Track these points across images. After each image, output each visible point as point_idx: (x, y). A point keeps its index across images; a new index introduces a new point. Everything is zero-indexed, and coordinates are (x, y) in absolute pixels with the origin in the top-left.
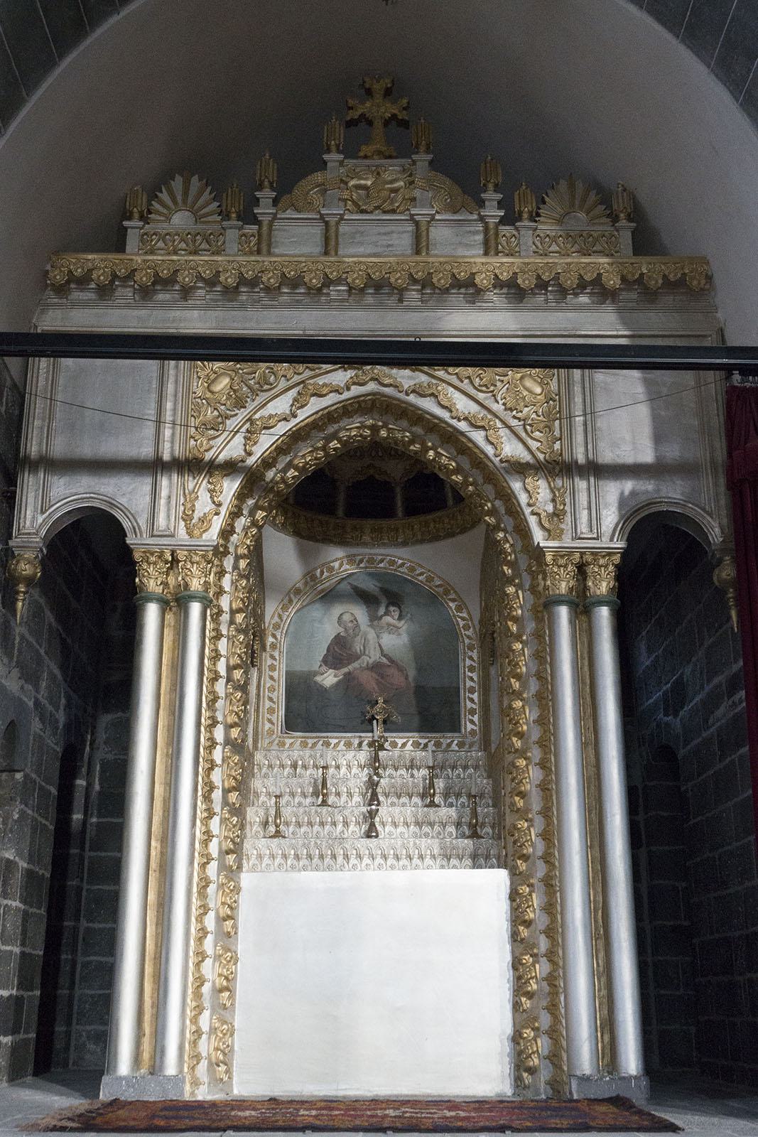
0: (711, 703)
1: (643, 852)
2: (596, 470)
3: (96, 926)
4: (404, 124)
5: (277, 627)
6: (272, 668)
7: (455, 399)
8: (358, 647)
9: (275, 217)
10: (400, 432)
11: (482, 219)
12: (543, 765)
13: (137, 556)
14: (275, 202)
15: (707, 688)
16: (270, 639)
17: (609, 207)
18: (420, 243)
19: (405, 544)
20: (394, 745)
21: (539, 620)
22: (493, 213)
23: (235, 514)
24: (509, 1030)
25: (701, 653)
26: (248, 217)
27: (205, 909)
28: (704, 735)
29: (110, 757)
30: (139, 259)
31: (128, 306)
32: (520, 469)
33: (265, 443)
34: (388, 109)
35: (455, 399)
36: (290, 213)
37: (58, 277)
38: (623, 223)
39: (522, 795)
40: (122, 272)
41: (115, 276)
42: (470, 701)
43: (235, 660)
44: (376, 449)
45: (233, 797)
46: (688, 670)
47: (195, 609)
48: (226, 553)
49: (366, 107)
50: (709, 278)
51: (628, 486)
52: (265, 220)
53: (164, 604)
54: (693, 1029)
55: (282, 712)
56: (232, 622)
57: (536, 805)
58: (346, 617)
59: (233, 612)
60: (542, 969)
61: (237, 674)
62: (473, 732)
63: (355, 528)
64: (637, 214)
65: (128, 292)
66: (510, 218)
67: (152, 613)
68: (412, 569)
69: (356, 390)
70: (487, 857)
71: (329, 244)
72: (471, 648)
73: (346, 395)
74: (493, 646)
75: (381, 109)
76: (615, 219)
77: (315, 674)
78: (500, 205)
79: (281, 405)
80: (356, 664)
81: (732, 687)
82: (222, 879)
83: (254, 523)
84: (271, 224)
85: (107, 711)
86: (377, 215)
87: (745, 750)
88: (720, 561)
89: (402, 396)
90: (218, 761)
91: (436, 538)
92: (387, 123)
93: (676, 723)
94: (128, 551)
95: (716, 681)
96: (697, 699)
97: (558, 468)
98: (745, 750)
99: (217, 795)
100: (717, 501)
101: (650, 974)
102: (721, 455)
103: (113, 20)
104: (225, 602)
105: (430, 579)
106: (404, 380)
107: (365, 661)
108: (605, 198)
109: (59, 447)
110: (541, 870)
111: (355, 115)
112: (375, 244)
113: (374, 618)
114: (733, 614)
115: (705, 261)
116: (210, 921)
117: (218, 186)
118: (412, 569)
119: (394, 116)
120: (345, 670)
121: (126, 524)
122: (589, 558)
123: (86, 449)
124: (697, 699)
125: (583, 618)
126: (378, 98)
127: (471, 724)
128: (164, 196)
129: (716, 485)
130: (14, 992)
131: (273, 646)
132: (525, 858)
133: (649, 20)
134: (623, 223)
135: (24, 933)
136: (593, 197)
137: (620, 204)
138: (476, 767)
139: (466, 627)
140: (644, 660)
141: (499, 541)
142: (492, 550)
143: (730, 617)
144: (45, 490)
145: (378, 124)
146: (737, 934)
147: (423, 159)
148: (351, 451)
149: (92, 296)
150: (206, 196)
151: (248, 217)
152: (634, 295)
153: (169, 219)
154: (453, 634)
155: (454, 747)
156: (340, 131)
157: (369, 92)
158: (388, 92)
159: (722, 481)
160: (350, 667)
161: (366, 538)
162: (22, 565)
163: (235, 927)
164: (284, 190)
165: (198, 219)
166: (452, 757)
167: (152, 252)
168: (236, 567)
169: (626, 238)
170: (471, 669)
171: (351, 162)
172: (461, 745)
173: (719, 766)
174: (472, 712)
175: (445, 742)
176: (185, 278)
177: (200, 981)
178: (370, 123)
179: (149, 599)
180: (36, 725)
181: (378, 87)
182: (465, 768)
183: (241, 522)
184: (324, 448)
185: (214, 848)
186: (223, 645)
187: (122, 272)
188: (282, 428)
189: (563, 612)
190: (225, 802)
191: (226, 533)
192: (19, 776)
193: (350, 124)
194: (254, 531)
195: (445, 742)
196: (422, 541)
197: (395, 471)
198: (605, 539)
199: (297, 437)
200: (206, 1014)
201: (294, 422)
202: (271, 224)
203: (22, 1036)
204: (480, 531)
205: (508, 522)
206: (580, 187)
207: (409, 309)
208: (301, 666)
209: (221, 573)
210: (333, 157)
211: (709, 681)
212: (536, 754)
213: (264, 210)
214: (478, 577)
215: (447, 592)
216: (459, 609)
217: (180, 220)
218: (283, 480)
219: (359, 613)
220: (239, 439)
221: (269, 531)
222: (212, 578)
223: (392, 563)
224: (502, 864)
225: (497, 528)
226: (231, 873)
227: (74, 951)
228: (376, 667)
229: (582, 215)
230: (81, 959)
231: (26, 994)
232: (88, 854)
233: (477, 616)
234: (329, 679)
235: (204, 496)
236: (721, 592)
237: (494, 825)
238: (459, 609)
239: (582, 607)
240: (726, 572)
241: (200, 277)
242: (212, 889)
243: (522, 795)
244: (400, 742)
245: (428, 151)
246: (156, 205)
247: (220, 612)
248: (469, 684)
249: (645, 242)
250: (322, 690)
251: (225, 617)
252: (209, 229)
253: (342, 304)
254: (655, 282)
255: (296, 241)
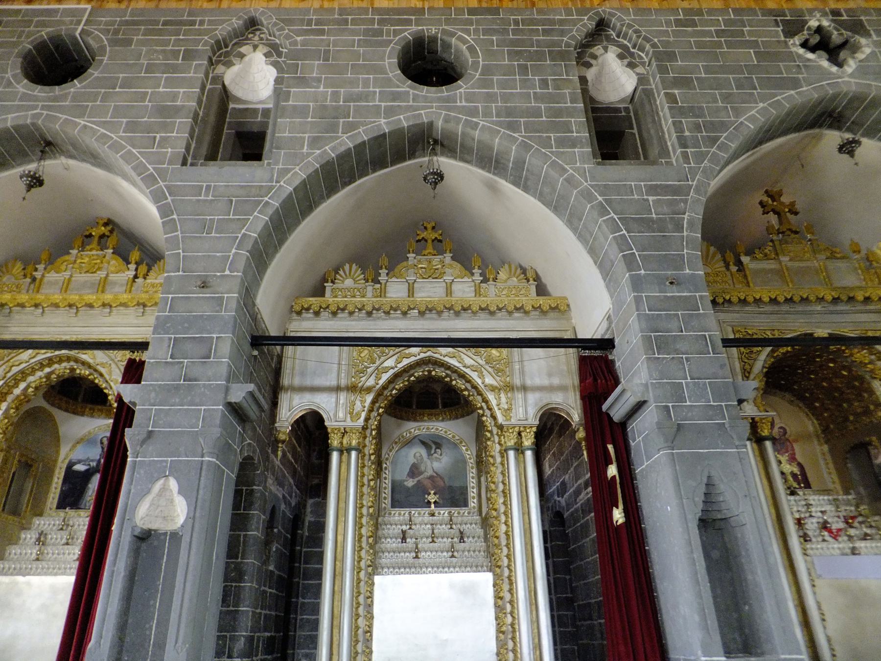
0: (577, 493)
1: (550, 561)
2: (524, 388)
3: (306, 601)
4: (440, 241)
5: (387, 459)
6: (385, 478)
7: (464, 360)
8: (423, 468)
9: (387, 281)
10: (439, 372)
11: (473, 281)
12: (506, 523)
13: (329, 430)
14: (387, 274)
15: (576, 486)
16: (384, 465)
17: (526, 275)
18: (449, 292)
19: (443, 420)
20: (439, 513)
21: (502, 457)
22: (478, 278)
23: (371, 411)
24: (495, 650)
25: (572, 469)
26: (376, 281)
27: (359, 593)
28: (575, 507)
29: (312, 519)
30: (331, 300)
31: (326, 320)
32: (493, 389)
33: (385, 377)
34: (434, 235)
35: (464, 360)
36: (394, 279)
37: (298, 308)
38: (531, 282)
39: (497, 537)
40: (324, 306)
41: (321, 307)
42: (472, 493)
43: (371, 477)
44: (430, 379)
45: (371, 540)
46: (567, 477)
47: (354, 454)
48: (367, 428)
49: (424, 234)
50: (568, 306)
51: (537, 395)
52: (383, 282)
53: (341, 452)
54: (576, 648)
55: (390, 499)
56: (370, 459)
57: (504, 542)
58: (418, 455)
59: (370, 455)
60: (509, 619)
61: (372, 483)
62: (474, 507)
63: (420, 415)
64: (537, 278)
65: (327, 313)
66: (485, 280)
67: (335, 456)
68: (446, 432)
69: (422, 355)
70: (482, 567)
71: (411, 292)
72: (472, 468)
73: (418, 357)
74: (482, 465)
75: (431, 235)
76: (528, 281)
77: (404, 481)
78: (481, 275)
79: (390, 363)
80: (422, 477)
81: (586, 486)
82: (366, 579)
83: (379, 414)
84: (386, 284)
85: (311, 498)
86: (430, 280)
87: (593, 514)
88: (578, 429)
89: (442, 358)
90: (364, 523)
91: (457, 418)
92: (433, 241)
93: (563, 501)
94: (325, 428)
95: (579, 482)
96: (571, 490)
97: (509, 388)
98: (593, 514)
99: (364, 539)
100: (576, 402)
101: (556, 620)
102: (577, 382)
103: (324, 205)
104: (366, 451)
105: (454, 437)
106: (443, 353)
107: (427, 474)
108: (524, 271)
109: (297, 382)
110: (506, 572)
111: (420, 238)
112: (430, 291)
113: (430, 455)
114: (585, 453)
115: (565, 298)
116: (361, 599)
117: (363, 268)
118: (446, 432)
119: (436, 238)
120: (417, 479)
121: (325, 416)
122: (522, 429)
123: (308, 382)
124: (571, 490)
125: (521, 455)
126: (430, 230)
127: (473, 503)
128: (341, 272)
129: (575, 395)
130: (273, 634)
131: (386, 468)
132: (499, 567)
133: (539, 204)
134: (531, 282)
135: (276, 605)
136: (519, 271)
137: (530, 274)
138: (476, 524)
139: (470, 459)
140: (548, 471)
141: (229, 8)
142: (480, 427)
143: (583, 454)
144: (291, 401)
145: (430, 241)
146: (593, 601)
147: (448, 255)
148: (419, 380)
149: (311, 315)
150: (359, 272)
151: (376, 281)
152: (537, 313)
153: (343, 282)
154: (464, 462)
155: (466, 514)
156: (414, 244)
157: (426, 228)
158: (433, 228)
159: (578, 394)
160: (419, 478)
161: (426, 418)
162: (281, 435)
163: (372, 601)
164: (390, 270)
165: (355, 282)
166: (465, 519)
167: (336, 297)
168: (371, 434)
169: (533, 289)
170: (473, 478)
171: (419, 257)
172: (469, 513)
173: (582, 522)
174: (474, 498)
175: (462, 512)
176: (351, 308)
177: (357, 628)
178: (426, 241)
179: (333, 450)
180: (283, 506)
181: (429, 226)
182: (471, 524)
183: (374, 414)
184: (408, 380)
185: (363, 564)
186: (366, 470)
187: (324, 306)
188: (391, 372)
189: (511, 454)
190: (368, 542)
191: (367, 420)
192: (275, 530)
193: (418, 241)
194: (378, 418)
195: (462, 512)
196: (450, 419)
197: (438, 388)
198: (530, 420)
199: (396, 376)
200: (360, 644)
201: (396, 369)
202: (386, 284)
203: (275, 655)
204: (475, 415)
205: (488, 413)
206: (513, 267)
207: (444, 319)
208: (398, 477)
209: (365, 438)
210: (411, 256)
211: (576, 482)
212: (503, 518)
213: (383, 278)
214: (474, 435)
215: (461, 442)
216: (467, 450)
217: (349, 282)
218: (391, 395)
219: (423, 451)
220: (373, 377)
221: (385, 416)
222: (361, 440)
223: (437, 429)
224: (490, 571)
225: (483, 415)
226: (370, 576)
227: (296, 614)
228: (431, 478)
229: (515, 279)
230: (299, 617)
231: (277, 635)
232: (302, 566)
233: (475, 454)
234: (410, 483)
235: (358, 403)
236: (579, 443)
237: (494, 559)
238: (467, 450)
239: (519, 450)
240: (581, 434)
241: (356, 307)
242: (362, 584)
243: (497, 537)
244: (442, 512)
245: (450, 252)
246: (338, 276)
247: (364, 456)
248: (472, 484)
249: (542, 290)
250: (408, 489)
251: (367, 457)
252: (360, 286)
253: (414, 318)
254: (546, 308)
255: (396, 290)
